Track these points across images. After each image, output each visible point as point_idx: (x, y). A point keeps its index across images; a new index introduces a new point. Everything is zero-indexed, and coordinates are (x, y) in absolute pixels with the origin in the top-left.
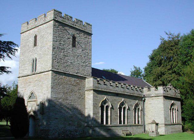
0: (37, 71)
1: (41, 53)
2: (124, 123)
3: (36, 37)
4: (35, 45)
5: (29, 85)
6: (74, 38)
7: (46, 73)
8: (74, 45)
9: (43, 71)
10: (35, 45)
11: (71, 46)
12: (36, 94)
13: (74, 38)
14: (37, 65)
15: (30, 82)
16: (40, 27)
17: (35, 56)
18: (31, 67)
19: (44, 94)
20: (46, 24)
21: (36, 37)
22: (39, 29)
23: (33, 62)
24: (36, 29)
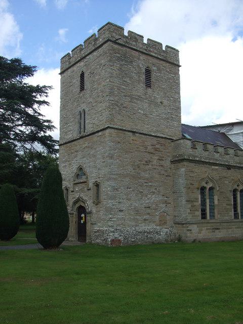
0: (89, 129)
1: (91, 100)
2: (212, 216)
3: (82, 75)
4: (82, 88)
5: (76, 157)
6: (148, 72)
7: (100, 134)
8: (148, 84)
9: (69, 145)
10: (82, 88)
11: (142, 86)
12: (87, 170)
13: (148, 72)
14: (87, 122)
15: (77, 151)
16: (88, 57)
17: (84, 106)
18: (76, 127)
19: (99, 169)
20: (71, 69)
21: (82, 75)
22: (86, 62)
23: (81, 115)
24: (82, 64)
